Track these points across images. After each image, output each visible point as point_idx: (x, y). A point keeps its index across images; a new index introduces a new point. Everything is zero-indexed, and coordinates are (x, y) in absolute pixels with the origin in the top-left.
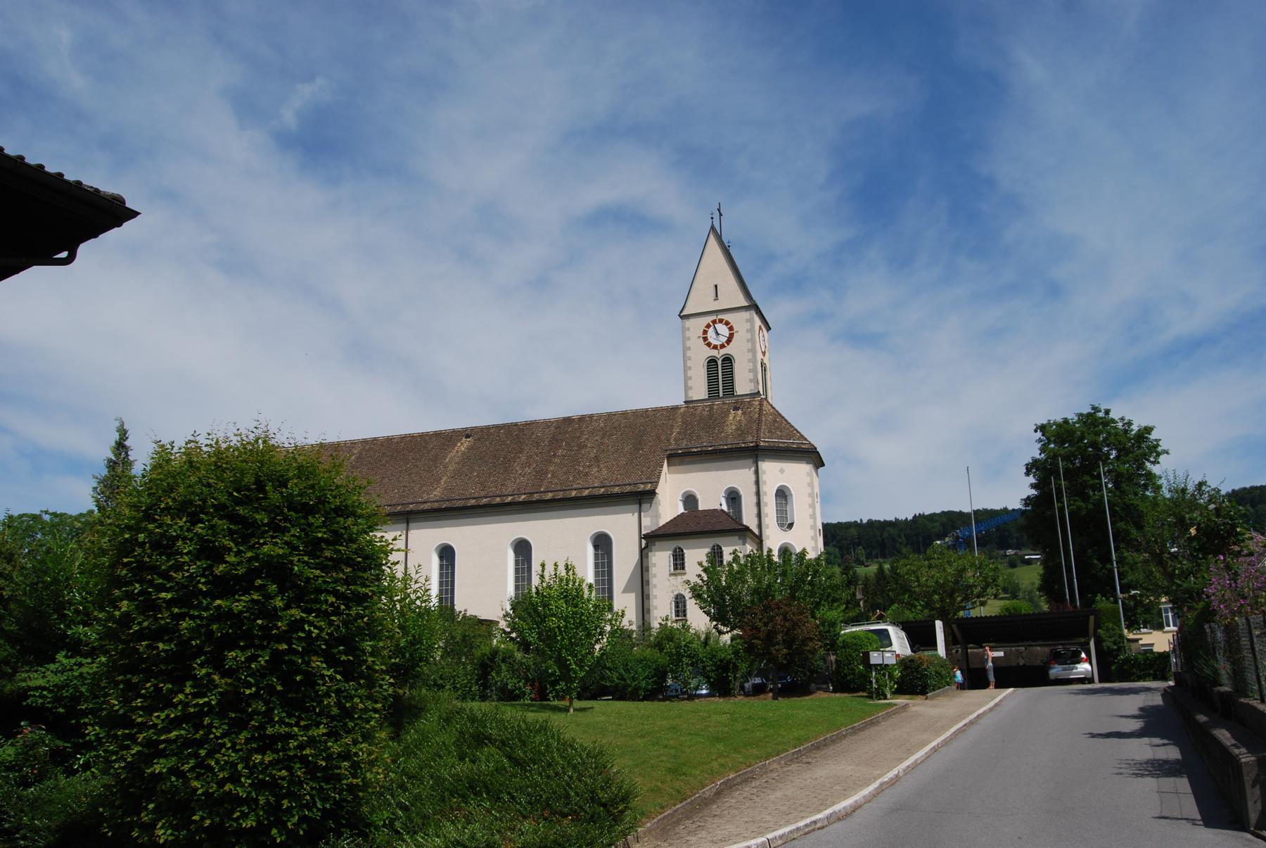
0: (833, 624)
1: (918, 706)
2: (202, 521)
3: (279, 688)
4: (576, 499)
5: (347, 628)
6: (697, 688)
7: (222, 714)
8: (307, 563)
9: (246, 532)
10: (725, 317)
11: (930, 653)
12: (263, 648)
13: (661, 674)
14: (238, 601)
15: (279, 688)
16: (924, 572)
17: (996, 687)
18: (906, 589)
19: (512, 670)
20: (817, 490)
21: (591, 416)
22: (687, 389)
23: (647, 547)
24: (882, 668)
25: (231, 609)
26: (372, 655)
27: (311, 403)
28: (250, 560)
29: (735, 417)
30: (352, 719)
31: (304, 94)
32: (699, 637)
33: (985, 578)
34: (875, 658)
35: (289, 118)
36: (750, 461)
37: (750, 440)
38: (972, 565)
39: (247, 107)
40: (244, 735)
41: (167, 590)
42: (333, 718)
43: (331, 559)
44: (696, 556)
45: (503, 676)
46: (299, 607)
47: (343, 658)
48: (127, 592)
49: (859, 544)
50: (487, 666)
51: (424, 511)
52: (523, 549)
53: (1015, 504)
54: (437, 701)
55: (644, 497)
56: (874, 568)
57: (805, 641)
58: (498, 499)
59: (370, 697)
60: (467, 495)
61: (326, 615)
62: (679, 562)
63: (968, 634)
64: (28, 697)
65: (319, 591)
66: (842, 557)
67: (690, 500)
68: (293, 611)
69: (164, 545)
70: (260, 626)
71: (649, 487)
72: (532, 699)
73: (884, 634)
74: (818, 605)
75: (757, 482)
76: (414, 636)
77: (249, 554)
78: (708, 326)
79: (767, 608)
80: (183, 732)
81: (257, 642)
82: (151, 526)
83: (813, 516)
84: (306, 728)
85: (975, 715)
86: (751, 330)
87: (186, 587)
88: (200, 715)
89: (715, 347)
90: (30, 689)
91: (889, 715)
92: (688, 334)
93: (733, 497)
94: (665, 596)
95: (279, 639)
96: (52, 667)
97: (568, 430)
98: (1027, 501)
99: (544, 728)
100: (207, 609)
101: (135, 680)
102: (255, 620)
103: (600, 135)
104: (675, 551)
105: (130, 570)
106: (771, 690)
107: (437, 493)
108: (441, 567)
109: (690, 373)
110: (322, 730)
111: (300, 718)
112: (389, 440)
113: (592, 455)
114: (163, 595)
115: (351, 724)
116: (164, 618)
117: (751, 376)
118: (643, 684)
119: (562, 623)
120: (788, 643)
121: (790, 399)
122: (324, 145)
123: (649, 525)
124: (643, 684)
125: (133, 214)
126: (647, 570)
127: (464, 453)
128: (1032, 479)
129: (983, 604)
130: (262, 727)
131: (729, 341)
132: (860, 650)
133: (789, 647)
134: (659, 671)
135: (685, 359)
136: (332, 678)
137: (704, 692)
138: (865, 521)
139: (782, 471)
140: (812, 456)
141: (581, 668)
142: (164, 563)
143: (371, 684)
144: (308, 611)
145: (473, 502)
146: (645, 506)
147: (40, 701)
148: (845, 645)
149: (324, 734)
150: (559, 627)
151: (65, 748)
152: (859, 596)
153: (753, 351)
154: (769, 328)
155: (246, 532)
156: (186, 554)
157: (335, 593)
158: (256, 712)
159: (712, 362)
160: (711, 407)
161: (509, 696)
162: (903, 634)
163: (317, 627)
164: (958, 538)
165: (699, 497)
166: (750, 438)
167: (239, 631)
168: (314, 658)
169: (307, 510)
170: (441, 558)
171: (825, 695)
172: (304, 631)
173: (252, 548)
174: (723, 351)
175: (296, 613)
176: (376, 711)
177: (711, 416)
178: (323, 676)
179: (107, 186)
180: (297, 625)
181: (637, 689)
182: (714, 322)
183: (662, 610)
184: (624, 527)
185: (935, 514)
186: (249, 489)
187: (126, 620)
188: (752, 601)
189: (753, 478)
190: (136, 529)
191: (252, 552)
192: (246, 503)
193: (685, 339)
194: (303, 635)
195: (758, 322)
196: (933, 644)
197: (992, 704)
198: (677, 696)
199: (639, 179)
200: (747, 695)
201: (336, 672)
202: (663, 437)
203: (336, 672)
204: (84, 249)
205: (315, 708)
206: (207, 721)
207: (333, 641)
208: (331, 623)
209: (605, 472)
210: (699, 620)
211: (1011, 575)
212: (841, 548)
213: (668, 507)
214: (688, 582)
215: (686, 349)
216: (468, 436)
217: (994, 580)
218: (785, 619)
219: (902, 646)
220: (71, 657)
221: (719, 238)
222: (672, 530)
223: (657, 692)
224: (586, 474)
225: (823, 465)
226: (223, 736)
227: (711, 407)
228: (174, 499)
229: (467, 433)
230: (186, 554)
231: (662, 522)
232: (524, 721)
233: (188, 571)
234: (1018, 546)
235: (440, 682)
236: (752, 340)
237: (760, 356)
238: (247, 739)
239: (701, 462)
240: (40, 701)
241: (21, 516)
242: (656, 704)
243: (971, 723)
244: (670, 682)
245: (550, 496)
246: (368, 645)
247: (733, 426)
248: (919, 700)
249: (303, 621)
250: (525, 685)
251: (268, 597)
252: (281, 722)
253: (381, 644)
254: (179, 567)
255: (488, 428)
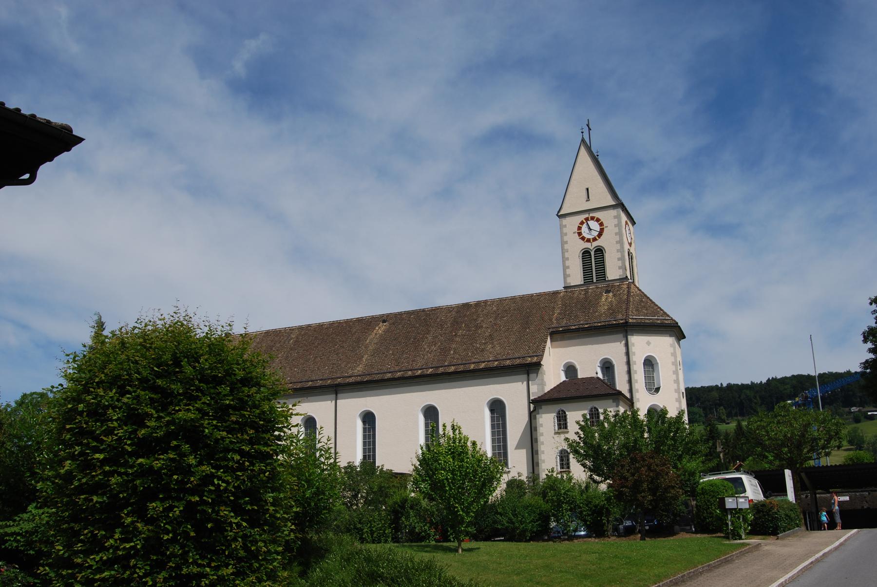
0: (692, 474)
1: (769, 546)
2: (129, 392)
3: (192, 534)
4: (474, 371)
5: (252, 482)
6: (576, 530)
7: (145, 557)
8: (216, 427)
9: (165, 400)
10: (596, 215)
11: (779, 498)
12: (179, 499)
13: (545, 519)
14: (158, 459)
15: (192, 534)
16: (775, 427)
17: (843, 528)
18: (760, 443)
19: (418, 514)
20: (679, 359)
21: (486, 302)
22: (566, 276)
23: (534, 410)
24: (737, 511)
25: (151, 467)
26: (273, 504)
27: (238, 292)
28: (168, 423)
29: (607, 299)
30: (258, 560)
31: (252, 47)
32: (580, 486)
33: (828, 432)
34: (730, 503)
35: (239, 67)
36: (621, 336)
37: (620, 318)
38: (816, 420)
39: (206, 61)
40: (164, 574)
41: (100, 452)
42: (240, 560)
43: (237, 422)
44: (575, 416)
45: (412, 521)
46: (209, 464)
47: (249, 507)
48: (69, 453)
49: (720, 405)
50: (399, 511)
51: (349, 384)
52: (431, 413)
53: (856, 368)
54: (340, 544)
55: (530, 368)
56: (733, 425)
57: (667, 489)
58: (410, 373)
59: (274, 542)
60: (384, 369)
61: (234, 470)
62: (562, 422)
63: (815, 481)
64: (7, 541)
65: (227, 450)
66: (706, 416)
67: (570, 370)
68: (204, 468)
69: (97, 413)
70: (177, 480)
71: (535, 359)
72: (437, 541)
73: (738, 482)
74: (680, 458)
75: (627, 354)
76: (318, 488)
77: (167, 419)
78: (582, 223)
79: (634, 460)
80: (113, 573)
81: (174, 495)
82: (88, 398)
83: (677, 381)
84: (217, 568)
85: (821, 554)
86: (619, 225)
87: (115, 448)
88: (128, 557)
89: (588, 240)
90: (7, 534)
91: (743, 554)
92: (565, 230)
93: (607, 367)
94: (545, 452)
95: (193, 492)
96: (25, 516)
97: (466, 313)
98: (866, 365)
99: (429, 567)
100: (132, 467)
101: (77, 527)
102: (172, 475)
103: (488, 70)
104: (558, 413)
105: (73, 435)
106: (640, 532)
107: (360, 369)
108: (364, 430)
109: (567, 263)
110: (230, 570)
111: (211, 560)
112: (320, 326)
113: (487, 334)
114: (97, 456)
115: (256, 565)
116: (98, 475)
117: (620, 263)
118: (530, 526)
119: (450, 476)
120: (653, 491)
121: (651, 283)
122: (267, 88)
123: (536, 391)
124: (530, 526)
125: (80, 140)
126: (536, 430)
127: (381, 336)
128: (870, 345)
129: (827, 454)
130: (178, 567)
131: (600, 234)
132: (716, 496)
133: (654, 495)
134: (541, 514)
135: (564, 251)
136: (239, 525)
137: (583, 533)
138: (725, 385)
139: (648, 343)
140: (674, 330)
141: (468, 513)
142: (98, 428)
143: (275, 528)
144: (217, 468)
145: (389, 375)
146: (532, 376)
147: (15, 544)
148: (704, 492)
149: (232, 574)
150: (447, 479)
151: (35, 584)
152: (719, 449)
153: (620, 242)
154: (634, 223)
155: (165, 400)
156: (116, 420)
157: (241, 453)
158: (173, 555)
159: (586, 253)
160: (586, 291)
161: (416, 538)
162: (756, 482)
163: (224, 482)
164: (806, 397)
165: (578, 367)
166: (620, 316)
167: (159, 486)
168: (223, 508)
169: (217, 381)
170: (364, 422)
171: (688, 536)
172: (213, 484)
173: (170, 414)
174: (595, 244)
175: (206, 469)
176: (278, 553)
177: (586, 298)
178: (231, 523)
179: (57, 119)
180: (207, 479)
181: (524, 531)
182: (587, 219)
183: (549, 462)
184: (515, 394)
185: (786, 378)
186: (167, 365)
187: (69, 477)
188: (621, 454)
189: (624, 350)
190: (77, 400)
191: (178, 416)
192: (166, 377)
193: (563, 234)
194: (212, 488)
195: (624, 218)
196: (784, 491)
197: (837, 543)
198: (559, 537)
199: (525, 103)
200: (619, 536)
201: (242, 519)
202: (546, 318)
203: (242, 519)
204: (44, 170)
205: (224, 551)
206: (132, 562)
207: (239, 493)
208: (238, 478)
209: (498, 348)
210: (579, 473)
211: (855, 430)
212: (704, 409)
213: (552, 374)
214: (567, 439)
215: (563, 243)
216: (384, 321)
217: (837, 433)
218: (649, 469)
219: (754, 492)
220: (40, 508)
221: (589, 149)
222: (556, 396)
223: (542, 534)
224: (483, 350)
225: (684, 337)
226: (146, 575)
227: (586, 291)
228: (106, 375)
229: (384, 319)
230: (116, 420)
231: (547, 389)
232: (412, 561)
233: (116, 435)
234: (862, 404)
235: (359, 526)
236: (620, 234)
237: (626, 247)
238: (165, 578)
239: (578, 337)
240: (15, 544)
241: (32, 394)
242: (541, 544)
243: (818, 561)
244: (553, 524)
245: (452, 369)
246: (270, 497)
247: (606, 307)
248: (771, 540)
249: (213, 476)
250: (430, 528)
251: (183, 455)
252: (195, 563)
253: (282, 495)
254: (110, 432)
255: (400, 314)
